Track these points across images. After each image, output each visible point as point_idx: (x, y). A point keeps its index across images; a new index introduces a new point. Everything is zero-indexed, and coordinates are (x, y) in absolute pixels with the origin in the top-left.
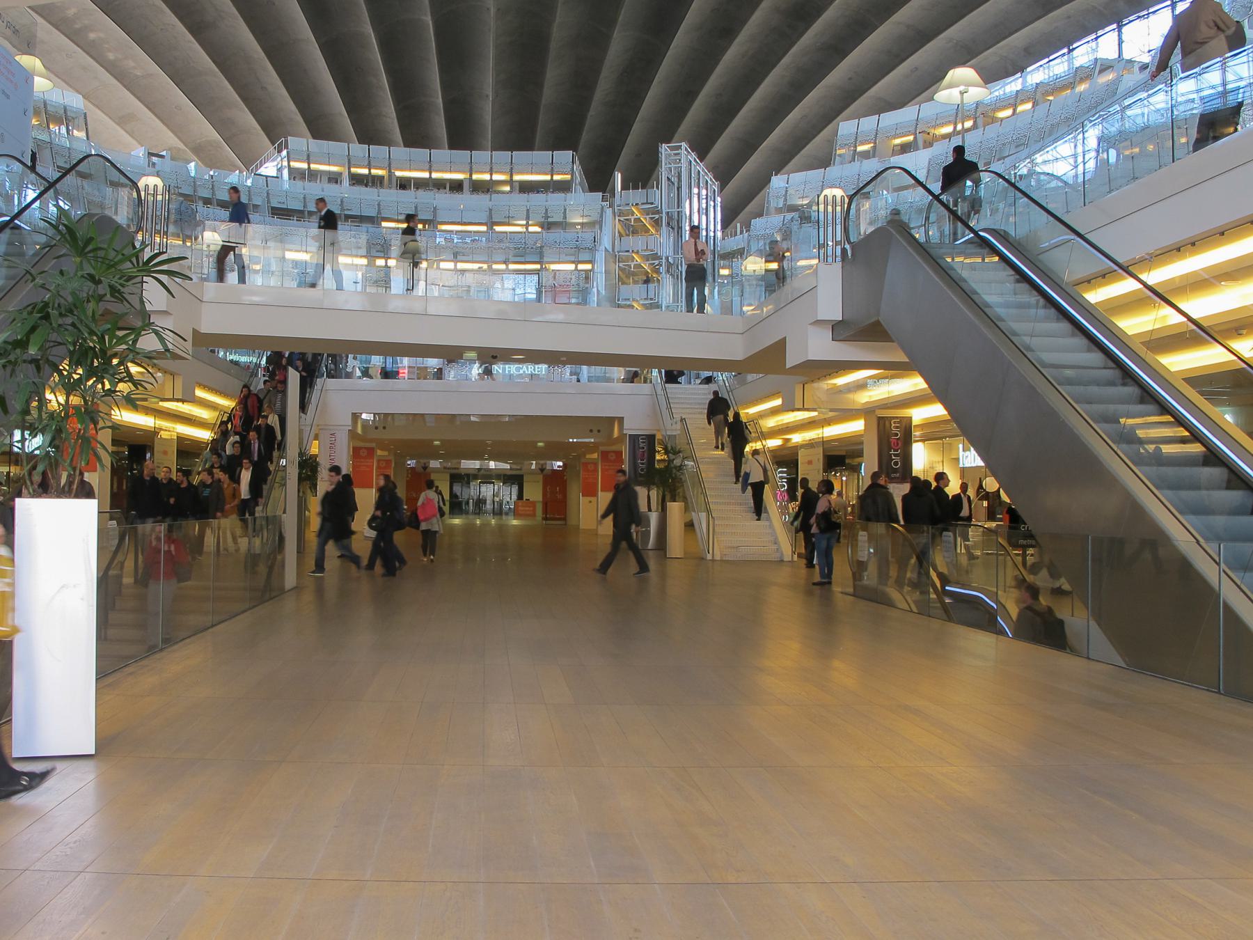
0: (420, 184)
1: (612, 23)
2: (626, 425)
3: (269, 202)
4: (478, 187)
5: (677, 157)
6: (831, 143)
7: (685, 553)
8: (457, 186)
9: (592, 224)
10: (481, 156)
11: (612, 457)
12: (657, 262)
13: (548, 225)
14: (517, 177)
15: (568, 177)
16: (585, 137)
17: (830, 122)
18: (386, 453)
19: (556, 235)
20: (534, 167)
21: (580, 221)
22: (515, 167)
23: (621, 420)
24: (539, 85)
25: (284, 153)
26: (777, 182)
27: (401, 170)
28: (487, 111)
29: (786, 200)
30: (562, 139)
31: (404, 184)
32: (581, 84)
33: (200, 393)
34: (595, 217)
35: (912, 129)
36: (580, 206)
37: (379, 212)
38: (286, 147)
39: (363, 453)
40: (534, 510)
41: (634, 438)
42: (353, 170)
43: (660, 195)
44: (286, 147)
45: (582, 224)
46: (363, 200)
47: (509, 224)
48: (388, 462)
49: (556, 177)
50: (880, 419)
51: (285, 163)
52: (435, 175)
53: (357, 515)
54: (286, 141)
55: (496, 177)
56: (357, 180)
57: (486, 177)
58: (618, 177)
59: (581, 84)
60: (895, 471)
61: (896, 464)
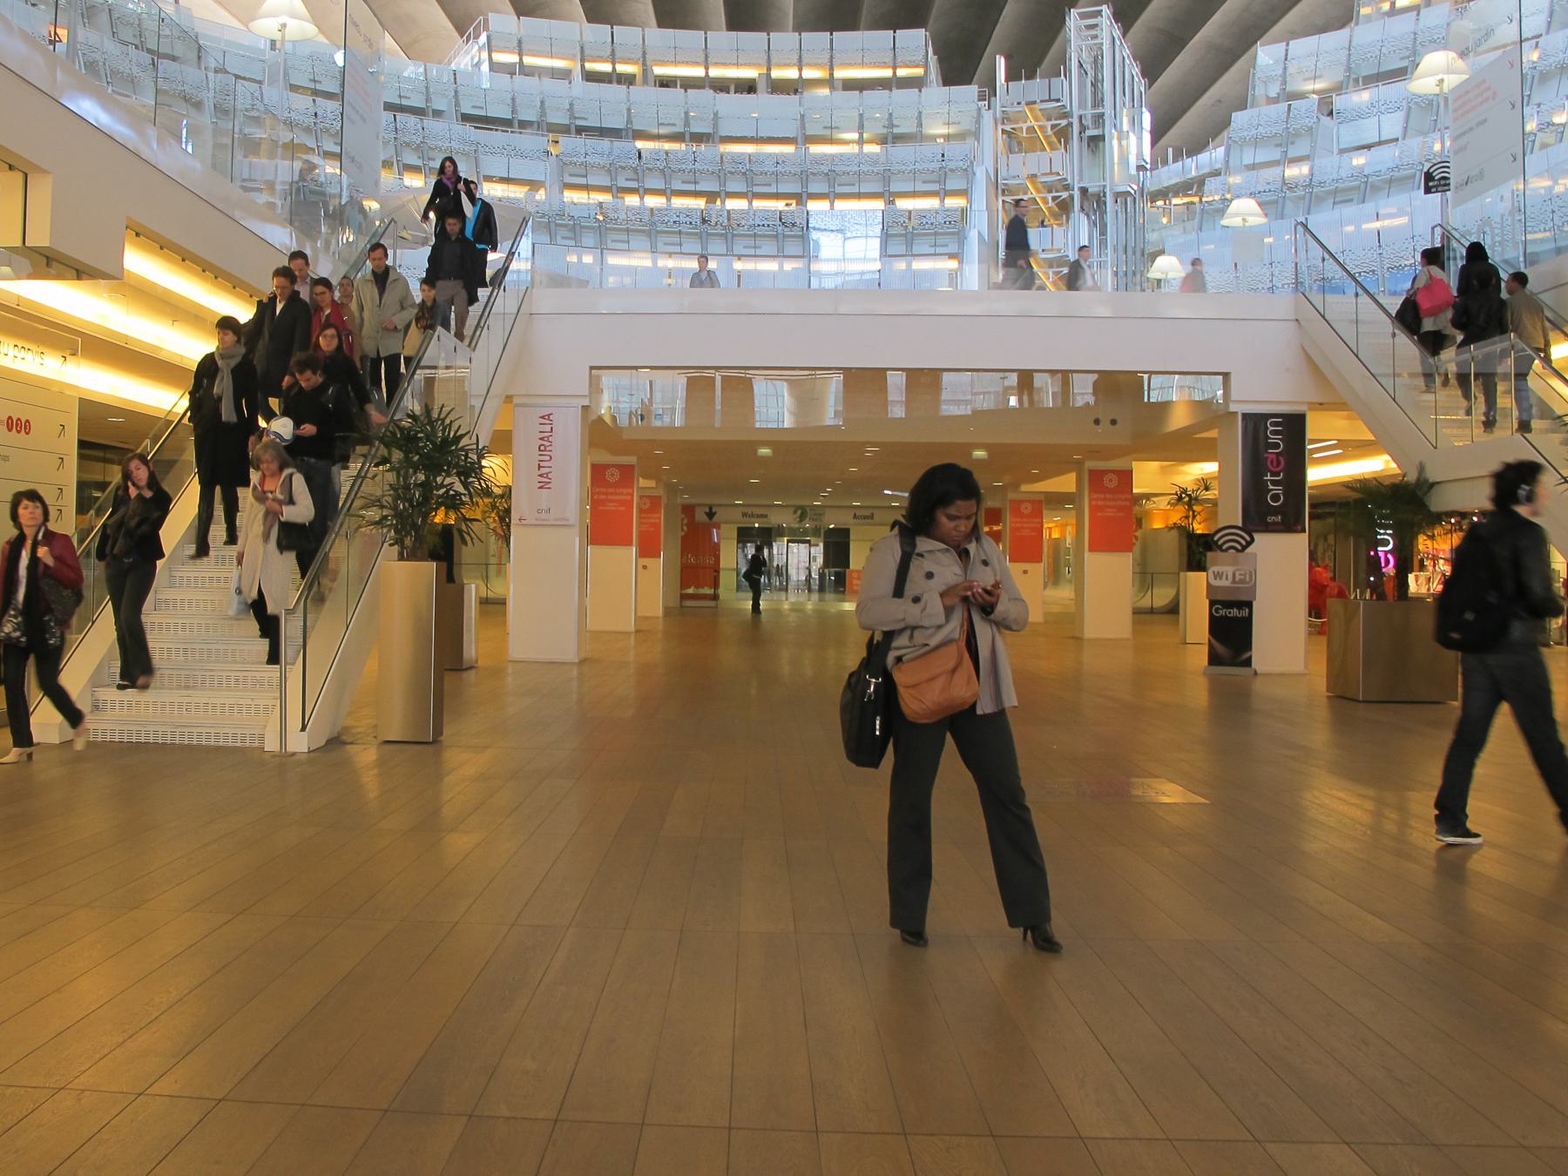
0: (689, 84)
3: (457, 104)
4: (779, 87)
6: (1246, 81)
7: (433, 556)
8: (749, 87)
9: (961, 136)
10: (785, 40)
11: (1111, 482)
14: (839, 74)
15: (919, 71)
17: (1235, 58)
18: (652, 484)
19: (902, 152)
20: (866, 54)
21: (944, 131)
22: (836, 55)
25: (483, 38)
26: (1266, 55)
27: (662, 63)
29: (1284, 82)
31: (665, 83)
33: (139, 262)
34: (967, 124)
36: (944, 110)
37: (629, 121)
38: (486, 28)
39: (613, 476)
41: (1255, 423)
42: (589, 66)
43: (1071, 91)
44: (486, 28)
45: (948, 137)
46: (608, 105)
47: (831, 141)
48: (655, 501)
49: (901, 72)
50: (1092, 473)
51: (485, 55)
52: (715, 72)
54: (486, 21)
55: (809, 73)
56: (591, 77)
57: (792, 73)
58: (1001, 63)
60: (1275, 511)
61: (1276, 498)
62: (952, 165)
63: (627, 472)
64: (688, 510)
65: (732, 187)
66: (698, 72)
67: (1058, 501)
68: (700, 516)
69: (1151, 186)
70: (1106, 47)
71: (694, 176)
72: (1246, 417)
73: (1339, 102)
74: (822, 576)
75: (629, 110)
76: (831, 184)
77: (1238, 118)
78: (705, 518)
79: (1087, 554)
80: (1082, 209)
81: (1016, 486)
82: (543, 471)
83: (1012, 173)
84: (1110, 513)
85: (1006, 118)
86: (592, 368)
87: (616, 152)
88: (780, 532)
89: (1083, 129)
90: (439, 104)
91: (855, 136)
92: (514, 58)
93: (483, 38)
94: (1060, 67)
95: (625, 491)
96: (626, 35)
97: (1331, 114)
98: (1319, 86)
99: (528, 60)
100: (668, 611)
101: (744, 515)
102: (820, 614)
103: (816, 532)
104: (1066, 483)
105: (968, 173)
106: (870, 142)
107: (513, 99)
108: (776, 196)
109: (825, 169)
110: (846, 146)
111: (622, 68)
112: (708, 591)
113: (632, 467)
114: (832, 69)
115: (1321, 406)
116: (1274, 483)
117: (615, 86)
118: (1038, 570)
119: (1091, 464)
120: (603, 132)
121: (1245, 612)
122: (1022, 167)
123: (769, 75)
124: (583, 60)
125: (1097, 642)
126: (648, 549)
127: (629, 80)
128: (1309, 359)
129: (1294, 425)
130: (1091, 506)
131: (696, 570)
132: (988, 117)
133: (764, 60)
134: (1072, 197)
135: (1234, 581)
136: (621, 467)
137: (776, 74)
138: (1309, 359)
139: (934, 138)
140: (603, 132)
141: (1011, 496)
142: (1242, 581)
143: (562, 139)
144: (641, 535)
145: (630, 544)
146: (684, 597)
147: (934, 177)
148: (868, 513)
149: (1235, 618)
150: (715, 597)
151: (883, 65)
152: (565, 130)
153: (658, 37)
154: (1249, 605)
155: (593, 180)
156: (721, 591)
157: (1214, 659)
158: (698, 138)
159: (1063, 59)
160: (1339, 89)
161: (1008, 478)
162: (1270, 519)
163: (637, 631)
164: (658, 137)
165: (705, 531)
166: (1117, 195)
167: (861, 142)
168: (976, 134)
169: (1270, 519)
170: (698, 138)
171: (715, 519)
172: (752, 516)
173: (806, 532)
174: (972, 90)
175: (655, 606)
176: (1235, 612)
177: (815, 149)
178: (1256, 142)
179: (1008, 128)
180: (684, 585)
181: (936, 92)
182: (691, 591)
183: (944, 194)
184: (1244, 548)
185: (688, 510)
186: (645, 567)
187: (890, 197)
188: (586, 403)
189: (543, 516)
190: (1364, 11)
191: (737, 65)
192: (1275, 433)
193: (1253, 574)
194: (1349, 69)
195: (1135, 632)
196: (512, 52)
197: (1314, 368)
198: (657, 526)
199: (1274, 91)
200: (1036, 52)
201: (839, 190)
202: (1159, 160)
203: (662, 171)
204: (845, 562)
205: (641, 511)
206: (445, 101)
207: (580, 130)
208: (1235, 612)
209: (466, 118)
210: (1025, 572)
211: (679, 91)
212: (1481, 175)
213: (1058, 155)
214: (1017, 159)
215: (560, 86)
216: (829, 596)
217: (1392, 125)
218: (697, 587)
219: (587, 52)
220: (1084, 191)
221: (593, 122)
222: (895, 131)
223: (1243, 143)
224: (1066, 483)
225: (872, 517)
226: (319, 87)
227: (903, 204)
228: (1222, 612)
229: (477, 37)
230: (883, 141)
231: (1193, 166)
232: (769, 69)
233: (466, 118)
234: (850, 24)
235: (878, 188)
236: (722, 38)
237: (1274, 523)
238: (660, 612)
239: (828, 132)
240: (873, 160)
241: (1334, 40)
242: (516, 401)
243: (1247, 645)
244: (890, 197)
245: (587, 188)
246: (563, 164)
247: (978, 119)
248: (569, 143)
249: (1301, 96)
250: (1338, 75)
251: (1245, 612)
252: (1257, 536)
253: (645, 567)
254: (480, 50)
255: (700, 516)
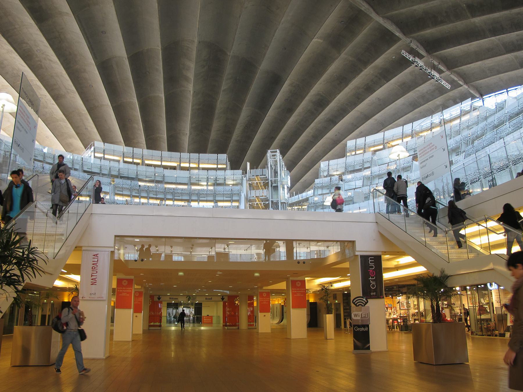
0: (155, 166)
1: (243, 102)
2: (358, 248)
3: (82, 167)
5: (274, 157)
8: (174, 168)
11: (299, 284)
12: (267, 202)
13: (216, 184)
14: (201, 166)
15: (225, 166)
16: (230, 149)
19: (220, 188)
21: (232, 183)
22: (200, 160)
23: (353, 242)
24: (209, 130)
25: (92, 149)
26: (323, 164)
27: (148, 160)
28: (186, 140)
29: (328, 172)
30: (220, 149)
32: (227, 131)
35: (382, 142)
36: (232, 177)
37: (137, 175)
39: (125, 283)
40: (212, 321)
41: (365, 259)
42: (125, 159)
43: (268, 173)
44: (94, 146)
45: (233, 185)
47: (199, 185)
48: (140, 293)
49: (219, 166)
50: (292, 281)
51: (93, 154)
52: (164, 163)
53: (209, 168)
55: (192, 165)
57: (187, 165)
58: (248, 164)
59: (227, 131)
61: (373, 286)
62: (235, 192)
63: (130, 282)
64: (152, 297)
65: (169, 196)
66: (159, 163)
67: (278, 292)
68: (156, 299)
69: (290, 202)
70: (278, 161)
71: (156, 193)
72: (361, 256)
73: (344, 177)
74: (194, 318)
75: (137, 172)
76: (199, 197)
77: (317, 181)
78: (158, 300)
79: (292, 311)
80: (272, 207)
81: (261, 287)
82: (93, 277)
83: (252, 196)
84: (298, 295)
85: (250, 180)
86: (116, 236)
87: (132, 184)
88: (181, 304)
89: (272, 183)
90: (77, 167)
91: (206, 183)
92: (102, 155)
93: (92, 149)
94: (265, 166)
95: (129, 289)
96: (138, 151)
97: (342, 180)
98: (338, 173)
99: (106, 156)
100: (144, 331)
101: (170, 298)
102: (193, 330)
103: (192, 304)
104: (282, 285)
105: (239, 195)
106: (210, 185)
107: (101, 167)
108: (182, 200)
109: (196, 192)
110: (203, 187)
111: (135, 161)
112: (157, 324)
113: (132, 280)
114: (199, 164)
115: (385, 253)
116: (372, 280)
117: (133, 165)
118: (268, 315)
119: (291, 278)
120: (128, 178)
121: (366, 329)
122: (254, 194)
123: (180, 165)
124: (124, 157)
125: (296, 340)
126: (137, 310)
127: (138, 164)
128: (380, 233)
129: (378, 259)
130: (292, 292)
131: (154, 318)
132: (245, 179)
133: (179, 161)
134: (269, 203)
135: (362, 317)
136: (127, 280)
137: (183, 165)
138: (380, 233)
139: (229, 185)
140: (128, 178)
141: (260, 291)
142: (365, 317)
143: (116, 180)
144: (135, 305)
145: (131, 308)
146: (150, 326)
147: (228, 196)
148: (210, 297)
149: (363, 331)
150: (160, 326)
151: (214, 164)
152: (117, 177)
153: (146, 152)
154: (368, 326)
155: (124, 193)
156: (162, 324)
157: (356, 347)
158: (158, 182)
159: (267, 164)
160: (344, 174)
161: (259, 285)
162: (372, 294)
163: (132, 341)
164: (146, 181)
165: (157, 303)
166: (282, 203)
167: (207, 185)
168: (241, 184)
169: (372, 294)
170: (158, 182)
171: (161, 300)
172: (173, 299)
173: (188, 304)
174: (240, 171)
175: (139, 329)
176: (362, 329)
177: (194, 187)
178: (322, 188)
179: (250, 183)
180: (150, 322)
181: (229, 172)
182: (152, 324)
183: (232, 201)
184: (365, 305)
185: (152, 297)
186: (136, 316)
187: (216, 201)
188: (112, 250)
189: (93, 296)
190: (348, 154)
191: (171, 161)
192: (371, 262)
193: (368, 314)
194: (346, 168)
195: (308, 336)
196: (101, 153)
197: (383, 238)
198: (141, 302)
199: (325, 174)
200: (258, 161)
201: (201, 199)
202: (292, 195)
203: (146, 191)
204: (201, 314)
205: (135, 296)
206: (78, 166)
207: (122, 177)
208: (362, 329)
209: (85, 171)
210: (265, 316)
211: (153, 168)
212: (433, 173)
213: (265, 191)
214: (253, 192)
215: (116, 164)
216: (196, 325)
217: (359, 183)
218: (154, 322)
219: (125, 155)
220: (272, 202)
221: (125, 175)
222: (218, 182)
223: (319, 188)
224: (282, 285)
225: (211, 299)
226: (36, 158)
227: (220, 204)
228: (358, 329)
229: (90, 148)
230: (214, 185)
231: (304, 195)
232: (180, 163)
233: (85, 171)
234: (205, 152)
235: (211, 198)
236: (166, 154)
237: (373, 295)
238: (141, 332)
239: (197, 182)
240: (211, 190)
241: (341, 161)
242: (83, 248)
243: (368, 341)
244: (216, 201)
245: (122, 195)
246: (115, 187)
247: (242, 179)
248: (117, 181)
249: (334, 175)
250: (343, 170)
251: (366, 329)
252: (369, 300)
253: (136, 316)
254: (91, 152)
255: (156, 299)
